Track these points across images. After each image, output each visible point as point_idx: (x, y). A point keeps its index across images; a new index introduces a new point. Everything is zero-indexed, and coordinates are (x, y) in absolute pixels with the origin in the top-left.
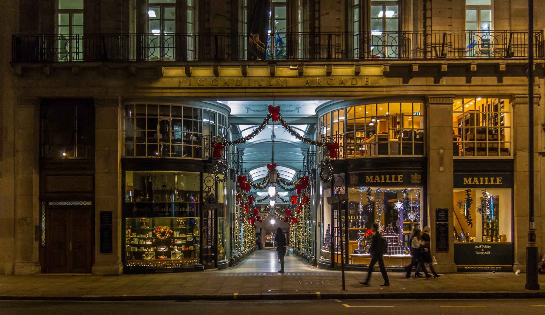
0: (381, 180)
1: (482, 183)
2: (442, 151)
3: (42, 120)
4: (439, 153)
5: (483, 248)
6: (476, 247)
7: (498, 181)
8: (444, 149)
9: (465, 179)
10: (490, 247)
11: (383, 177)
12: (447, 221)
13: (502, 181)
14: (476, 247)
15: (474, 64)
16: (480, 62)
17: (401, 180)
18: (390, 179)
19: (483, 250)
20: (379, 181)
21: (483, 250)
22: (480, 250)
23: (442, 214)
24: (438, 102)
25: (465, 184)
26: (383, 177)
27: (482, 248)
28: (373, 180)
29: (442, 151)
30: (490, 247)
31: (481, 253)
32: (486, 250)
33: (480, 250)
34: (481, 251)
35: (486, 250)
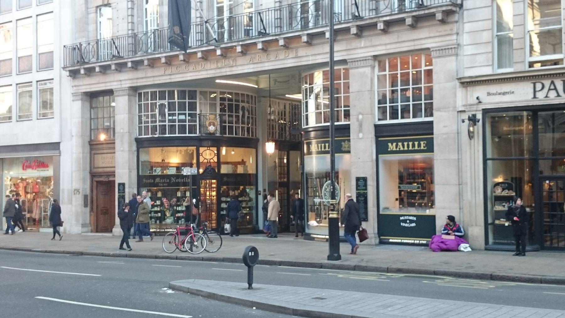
0: (404, 147)
1: (406, 148)
2: (360, 117)
3: (92, 110)
4: (358, 120)
5: (409, 220)
6: (402, 218)
7: (422, 145)
8: (362, 115)
9: (390, 144)
10: (415, 219)
11: (406, 144)
12: (366, 189)
13: (426, 145)
14: (402, 218)
15: (438, 12)
16: (444, 9)
17: (424, 147)
18: (413, 146)
19: (408, 221)
20: (402, 149)
21: (408, 221)
22: (405, 221)
23: (361, 183)
24: (357, 66)
25: (389, 150)
26: (406, 144)
27: (407, 220)
28: (396, 148)
29: (360, 117)
30: (415, 219)
31: (406, 225)
32: (412, 222)
33: (405, 221)
34: (406, 223)
35: (412, 222)
